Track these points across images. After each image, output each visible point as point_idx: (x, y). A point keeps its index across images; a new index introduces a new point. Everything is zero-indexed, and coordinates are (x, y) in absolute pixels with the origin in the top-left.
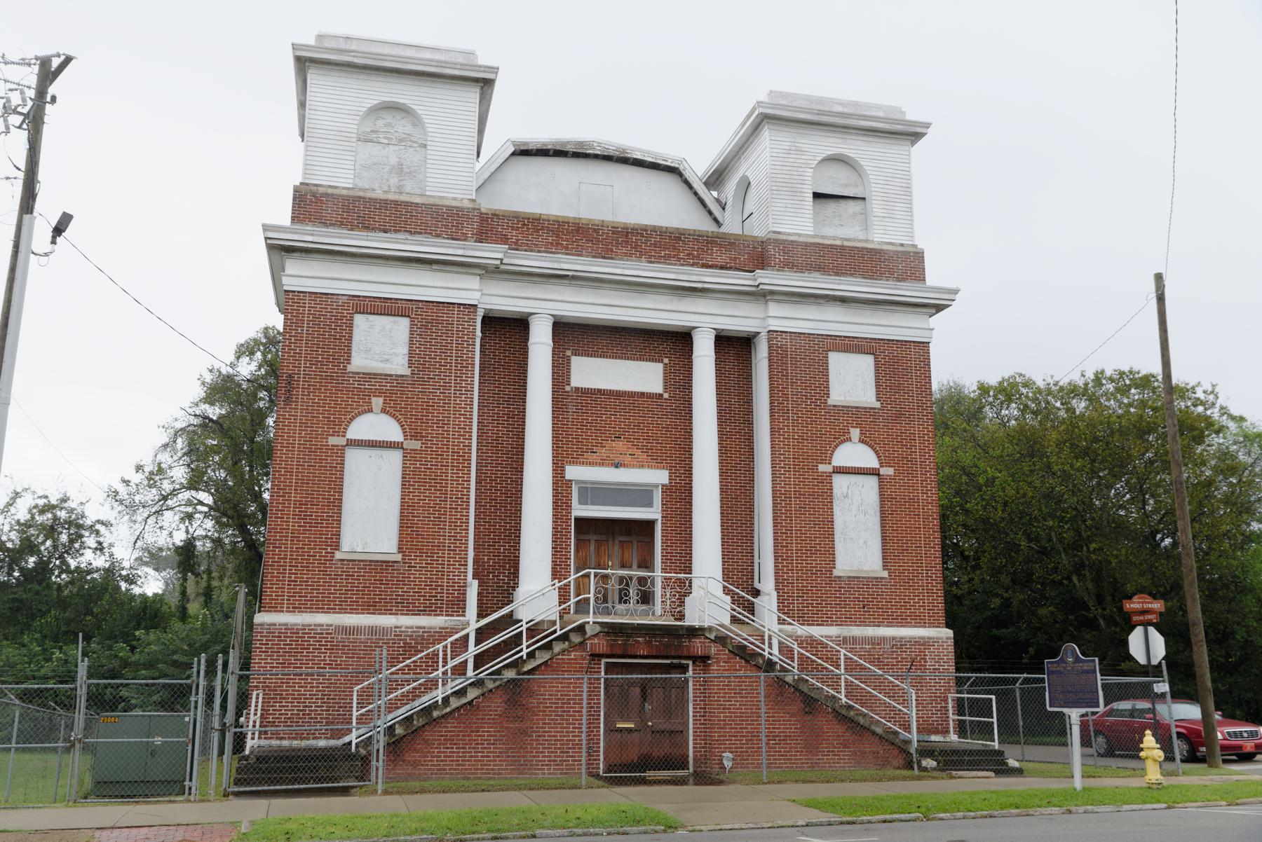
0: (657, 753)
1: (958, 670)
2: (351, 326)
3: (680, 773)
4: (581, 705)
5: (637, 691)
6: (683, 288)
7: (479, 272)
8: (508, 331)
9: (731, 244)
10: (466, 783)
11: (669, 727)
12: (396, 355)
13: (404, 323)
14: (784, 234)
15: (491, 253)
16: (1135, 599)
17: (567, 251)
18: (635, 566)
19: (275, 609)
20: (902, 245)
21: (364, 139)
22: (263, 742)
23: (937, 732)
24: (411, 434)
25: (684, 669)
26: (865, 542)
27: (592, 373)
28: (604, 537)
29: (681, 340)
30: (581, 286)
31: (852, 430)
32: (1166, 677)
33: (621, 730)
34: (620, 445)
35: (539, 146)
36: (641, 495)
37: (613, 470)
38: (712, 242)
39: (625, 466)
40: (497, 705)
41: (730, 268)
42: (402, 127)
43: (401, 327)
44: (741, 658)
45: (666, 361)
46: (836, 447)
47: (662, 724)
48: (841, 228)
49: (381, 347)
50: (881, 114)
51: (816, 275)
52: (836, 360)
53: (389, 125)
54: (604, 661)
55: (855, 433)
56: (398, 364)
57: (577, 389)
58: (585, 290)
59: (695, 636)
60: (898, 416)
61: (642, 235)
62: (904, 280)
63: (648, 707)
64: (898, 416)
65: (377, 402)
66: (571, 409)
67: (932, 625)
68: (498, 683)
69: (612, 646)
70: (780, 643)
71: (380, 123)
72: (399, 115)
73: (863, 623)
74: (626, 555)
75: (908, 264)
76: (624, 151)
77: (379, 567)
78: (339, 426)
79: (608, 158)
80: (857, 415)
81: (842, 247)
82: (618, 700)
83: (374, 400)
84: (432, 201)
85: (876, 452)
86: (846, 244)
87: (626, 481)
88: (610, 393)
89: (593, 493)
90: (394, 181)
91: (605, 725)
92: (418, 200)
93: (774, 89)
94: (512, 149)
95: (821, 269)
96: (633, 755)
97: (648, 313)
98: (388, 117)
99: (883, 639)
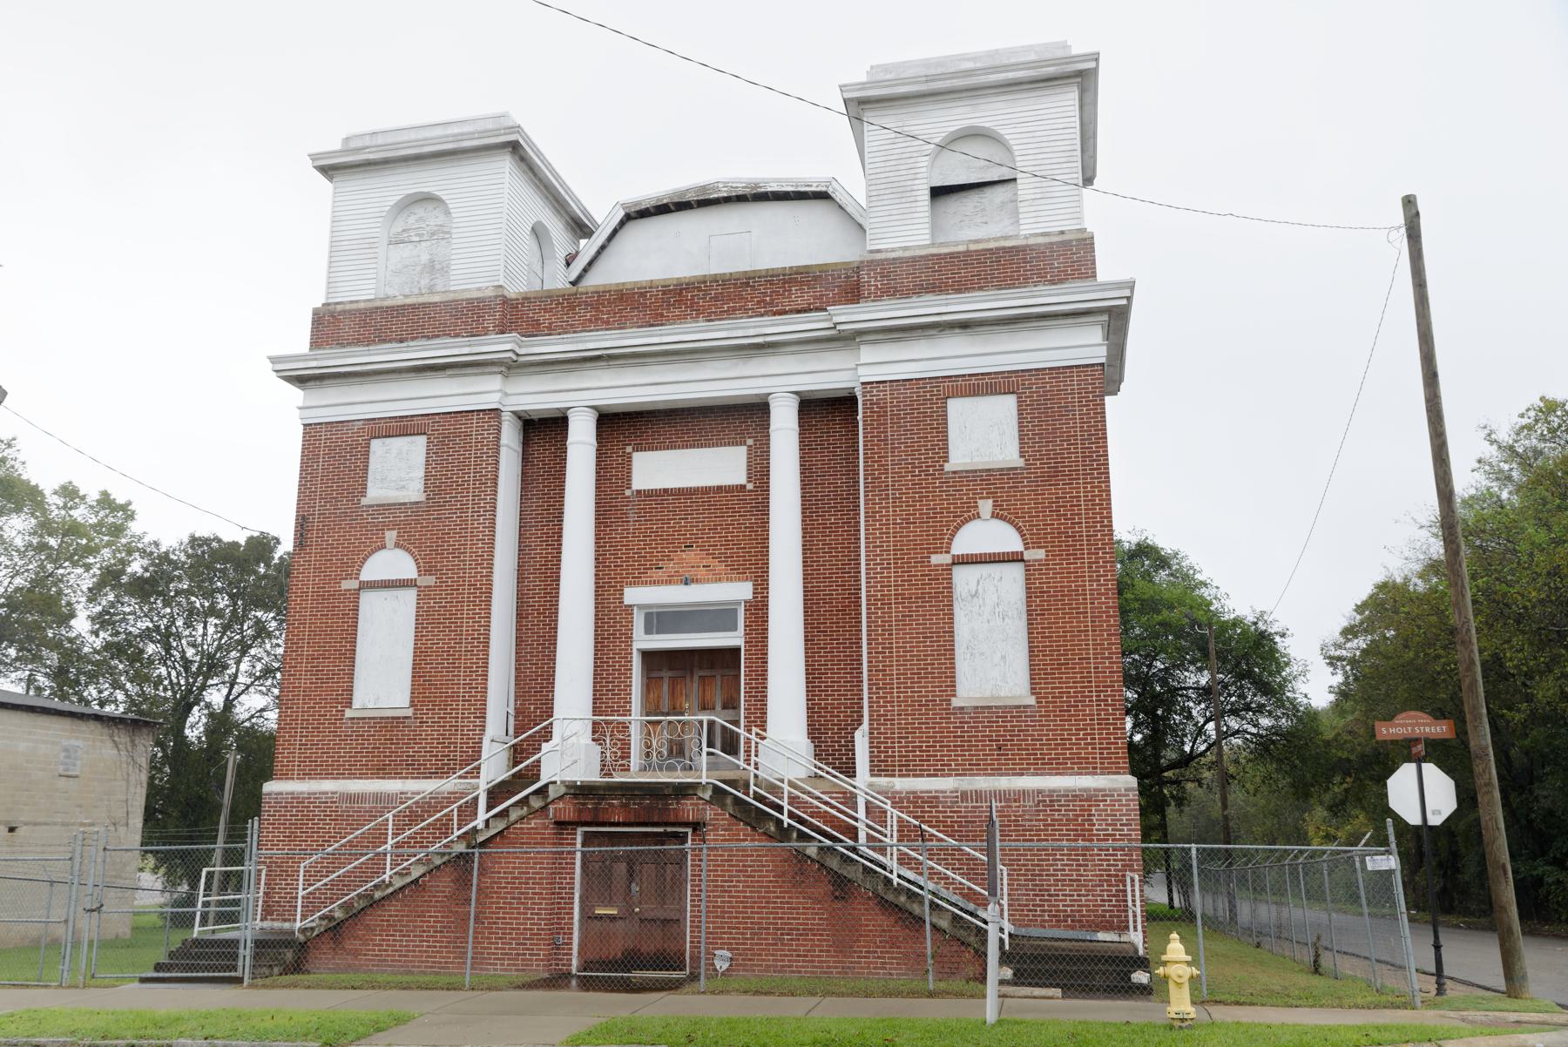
0: (648, 947)
1: (1146, 837)
2: (367, 453)
3: (675, 975)
4: (560, 888)
5: (622, 868)
6: (585, 360)
7: (496, 369)
8: (544, 431)
9: (816, 278)
10: (406, 978)
11: (661, 914)
12: (412, 479)
13: (1008, 404)
14: (887, 251)
15: (499, 345)
16: (1399, 720)
17: (608, 325)
18: (719, 708)
19: (286, 777)
20: (1062, 232)
21: (396, 242)
22: (267, 924)
23: (1108, 927)
24: (425, 569)
25: (682, 838)
26: (1004, 657)
27: (656, 469)
28: (679, 673)
29: (754, 413)
30: (623, 366)
31: (980, 502)
32: (1393, 846)
33: (600, 918)
34: (691, 556)
35: (653, 203)
36: (719, 617)
37: (683, 588)
38: (790, 281)
39: (697, 581)
40: (445, 884)
41: (810, 310)
42: (433, 218)
43: (1006, 406)
44: (746, 824)
45: (750, 442)
46: (957, 529)
47: (651, 909)
48: (975, 226)
49: (398, 471)
50: (1033, 57)
51: (930, 297)
52: (959, 411)
53: (421, 219)
54: (580, 830)
55: (986, 506)
56: (414, 491)
57: (639, 492)
58: (709, 364)
59: (685, 796)
60: (1053, 475)
61: (699, 289)
62: (1061, 281)
63: (635, 888)
64: (1053, 475)
65: (391, 536)
66: (632, 517)
67: (1106, 771)
68: (446, 858)
69: (580, 811)
70: (867, 803)
71: (412, 220)
72: (430, 206)
73: (997, 772)
74: (708, 694)
75: (1072, 257)
76: (756, 186)
77: (390, 724)
78: (352, 567)
79: (741, 199)
80: (989, 481)
81: (967, 253)
82: (598, 880)
83: (388, 534)
84: (451, 297)
85: (1019, 529)
86: (973, 247)
87: (684, 597)
88: (680, 492)
89: (661, 619)
90: (425, 282)
91: (582, 909)
92: (436, 299)
93: (875, 63)
94: (621, 214)
95: (936, 288)
96: (616, 950)
97: (661, 389)
98: (420, 211)
99: (1022, 794)
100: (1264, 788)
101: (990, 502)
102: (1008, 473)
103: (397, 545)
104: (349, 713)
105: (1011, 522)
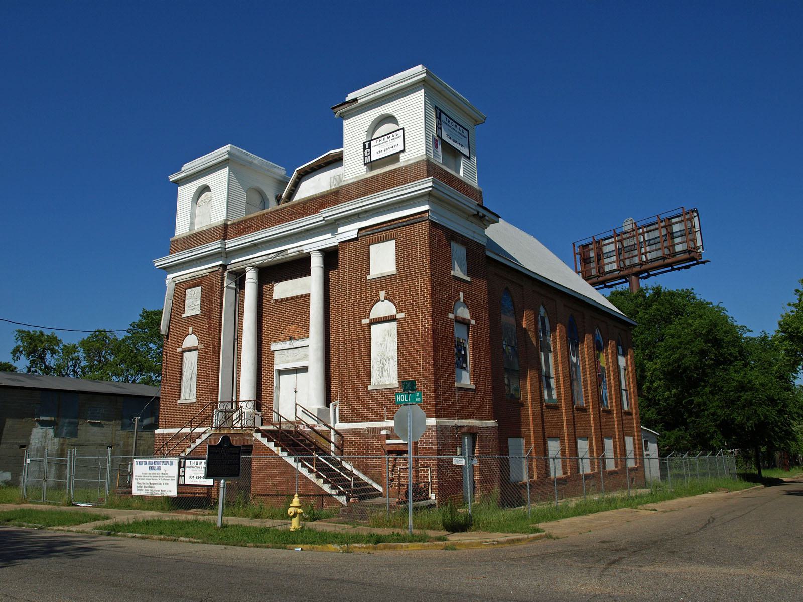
80: (385, 282)
100: (716, 407)
101: (384, 292)
102: (391, 277)
103: (386, 299)
104: (179, 402)
105: (391, 301)
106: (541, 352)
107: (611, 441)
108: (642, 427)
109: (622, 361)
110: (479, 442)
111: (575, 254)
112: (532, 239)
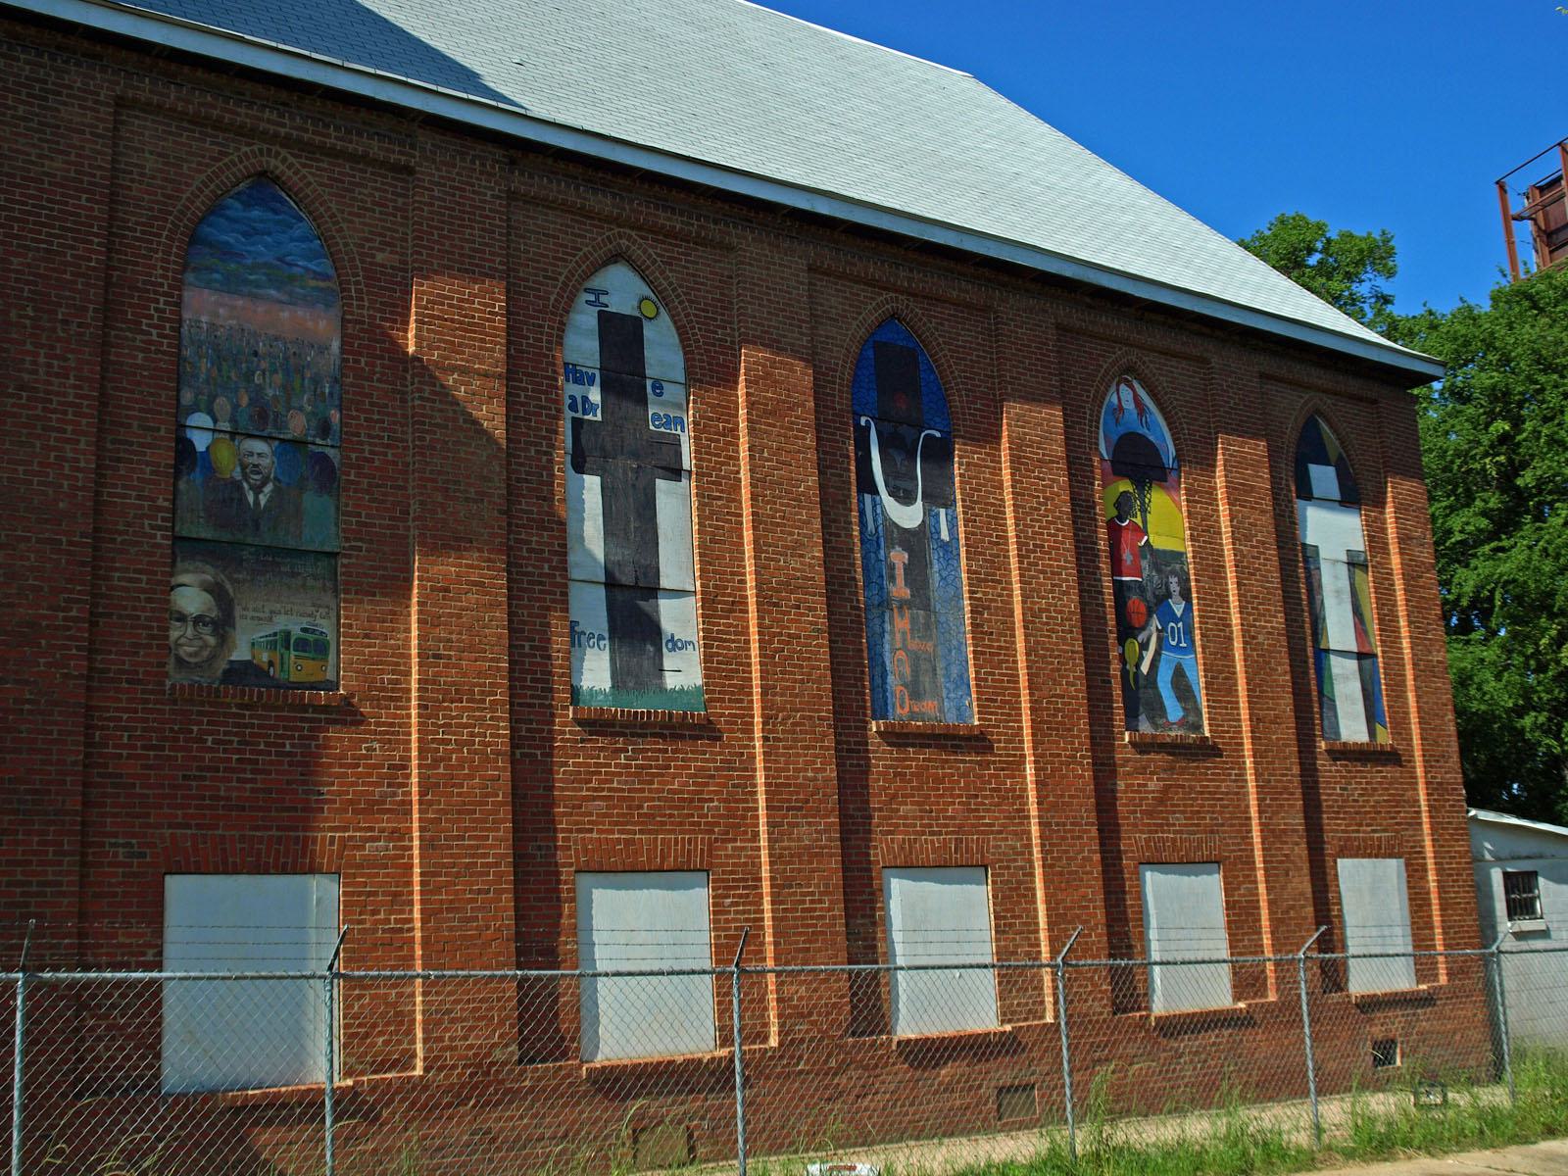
106: (580, 467)
107: (1210, 887)
108: (1473, 812)
109: (1332, 531)
110: (412, 929)
111: (1509, 219)
112: (958, 80)
